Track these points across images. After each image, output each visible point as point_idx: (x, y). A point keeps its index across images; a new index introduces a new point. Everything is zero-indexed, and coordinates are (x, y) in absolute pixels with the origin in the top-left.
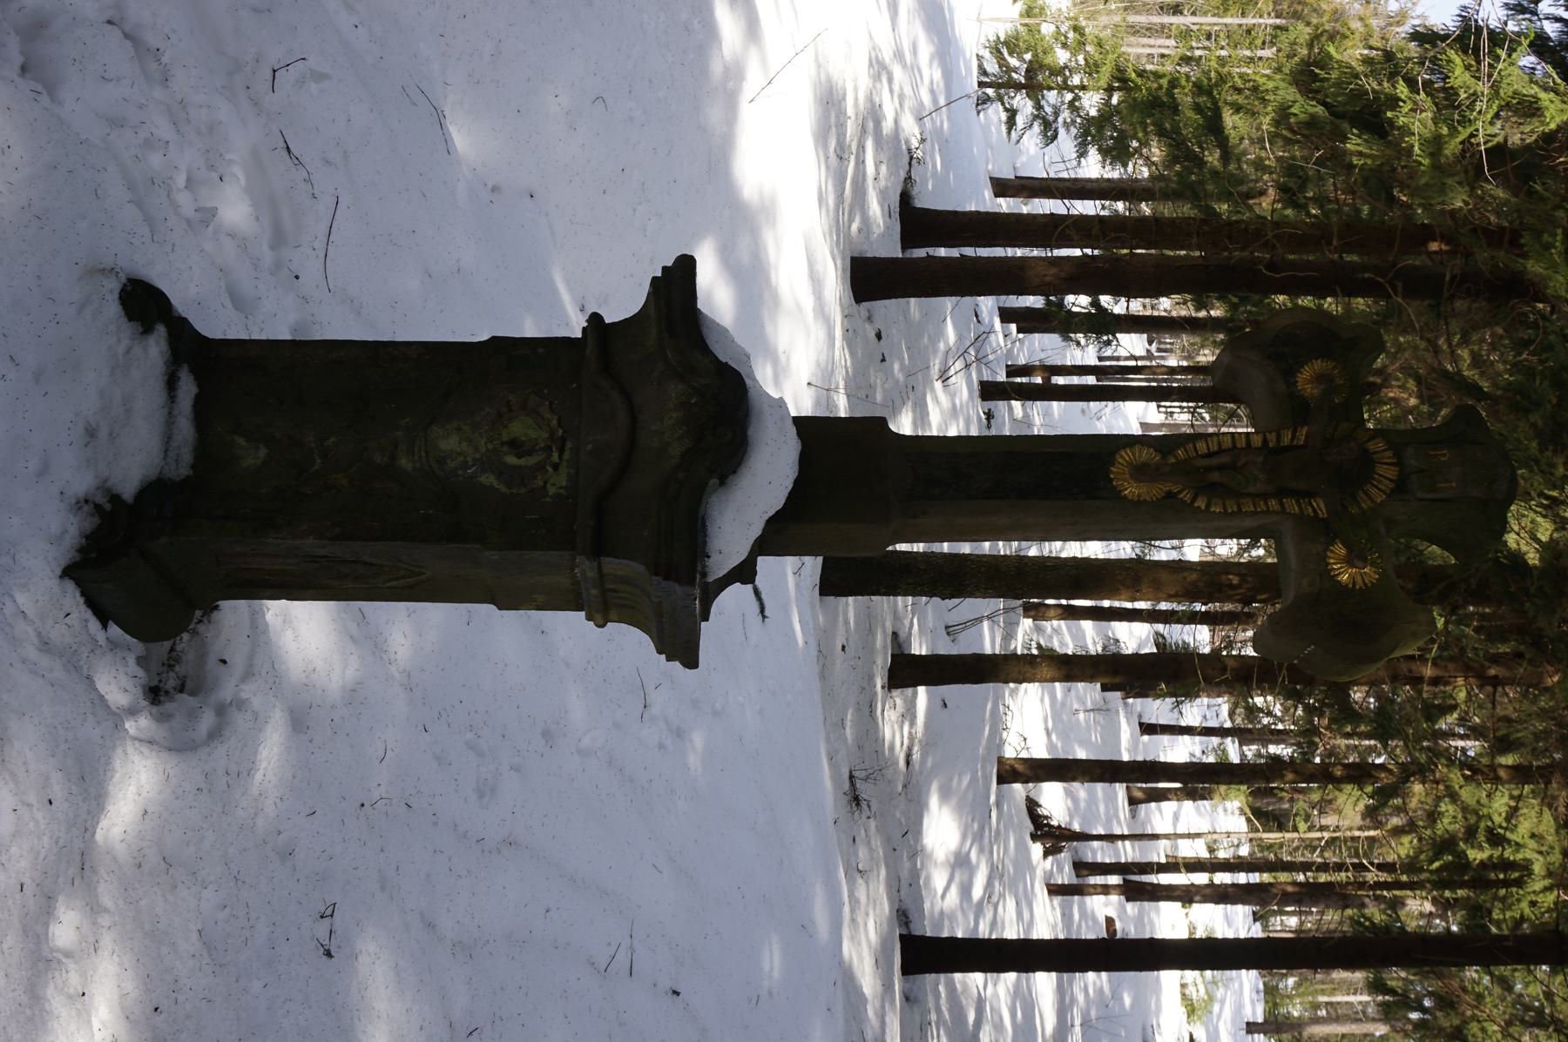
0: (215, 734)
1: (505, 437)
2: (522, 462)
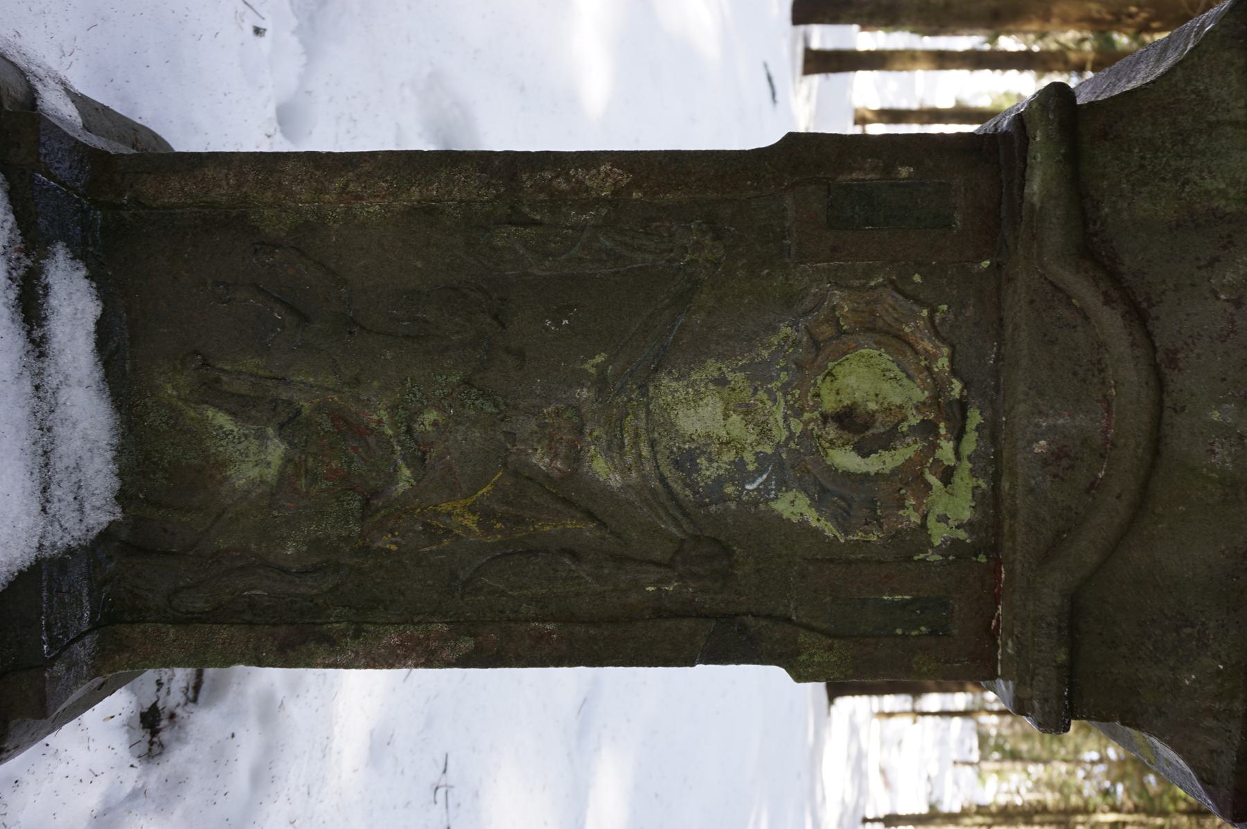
0: (262, 776)
1: (830, 404)
2: (871, 465)
